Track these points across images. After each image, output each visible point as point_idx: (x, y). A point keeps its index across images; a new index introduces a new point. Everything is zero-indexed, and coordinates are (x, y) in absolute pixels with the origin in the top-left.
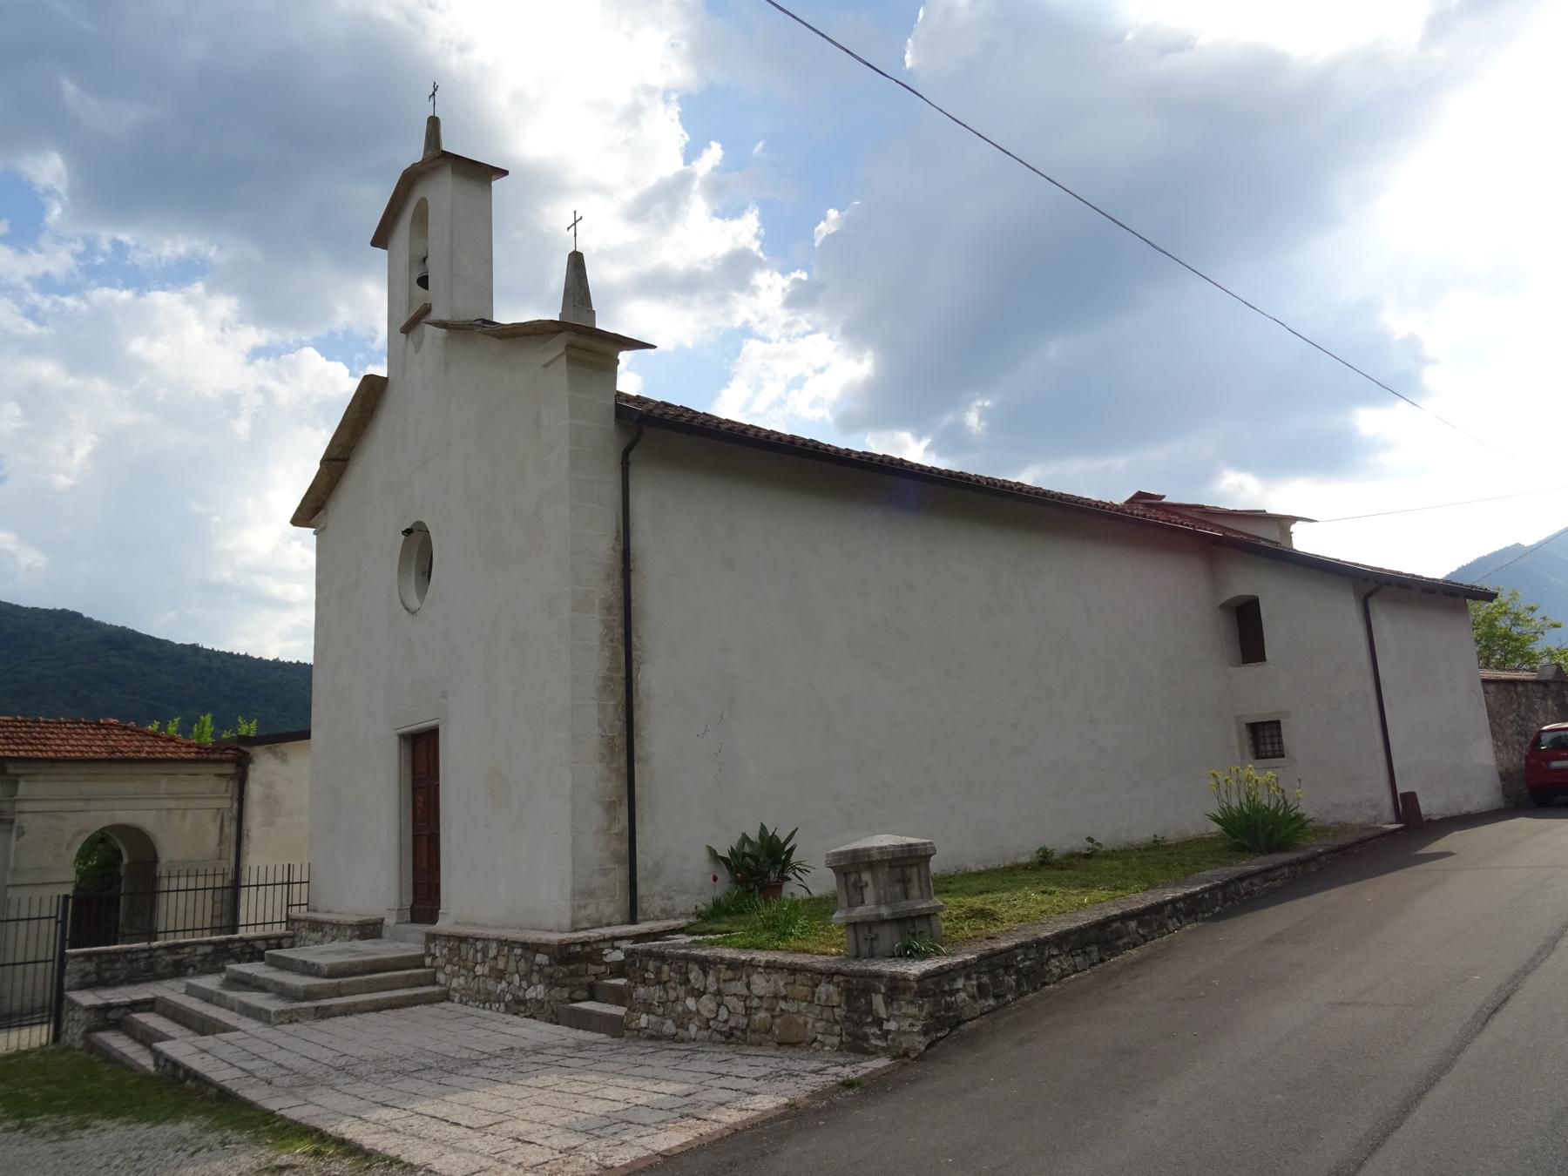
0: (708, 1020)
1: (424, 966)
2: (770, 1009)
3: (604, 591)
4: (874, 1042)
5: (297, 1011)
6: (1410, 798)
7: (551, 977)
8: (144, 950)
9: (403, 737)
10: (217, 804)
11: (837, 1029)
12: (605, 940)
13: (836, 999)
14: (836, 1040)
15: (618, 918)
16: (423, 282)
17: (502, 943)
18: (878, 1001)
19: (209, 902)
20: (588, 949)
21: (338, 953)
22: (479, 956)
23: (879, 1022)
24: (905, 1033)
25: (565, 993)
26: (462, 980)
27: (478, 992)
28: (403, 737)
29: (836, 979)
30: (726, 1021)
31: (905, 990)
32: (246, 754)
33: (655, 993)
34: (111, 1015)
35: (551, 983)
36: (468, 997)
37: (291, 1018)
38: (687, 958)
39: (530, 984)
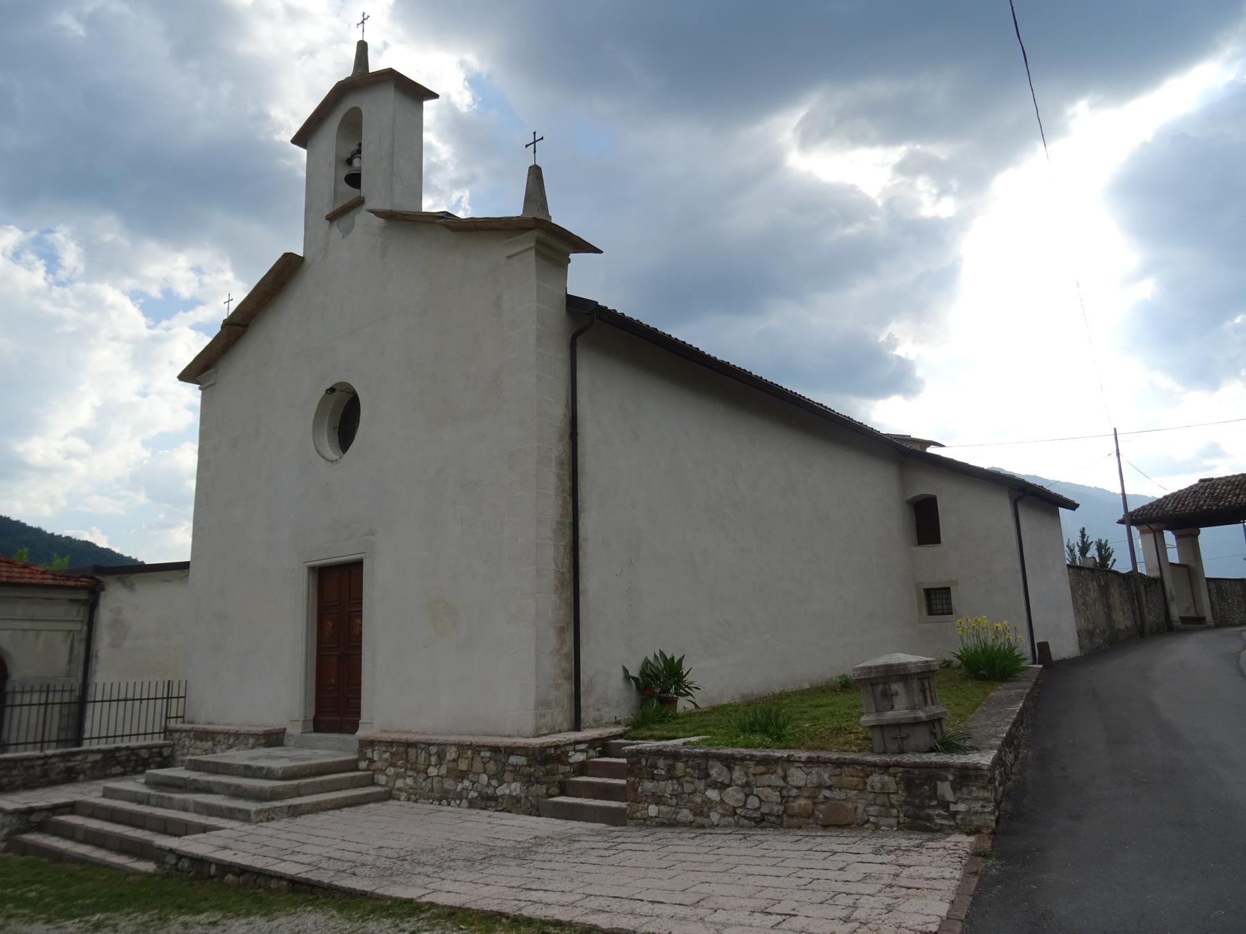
0: (734, 808)
1: (358, 770)
2: (813, 798)
3: (558, 449)
4: (939, 821)
5: (273, 810)
6: (1044, 647)
7: (530, 775)
8: (39, 758)
9: (312, 569)
10: (69, 626)
11: (894, 812)
12: (570, 744)
13: (892, 787)
14: (893, 821)
15: (566, 726)
16: (354, 180)
17: (461, 747)
18: (945, 789)
19: (56, 716)
20: (559, 752)
21: (293, 759)
22: (434, 759)
23: (945, 805)
24: (976, 813)
25: (543, 789)
26: (409, 781)
27: (432, 790)
28: (312, 569)
29: (892, 770)
30: (759, 808)
31: (977, 778)
32: (99, 582)
33: (669, 787)
34: (34, 818)
35: (529, 780)
36: (415, 795)
37: (269, 816)
38: (707, 756)
39: (501, 783)
